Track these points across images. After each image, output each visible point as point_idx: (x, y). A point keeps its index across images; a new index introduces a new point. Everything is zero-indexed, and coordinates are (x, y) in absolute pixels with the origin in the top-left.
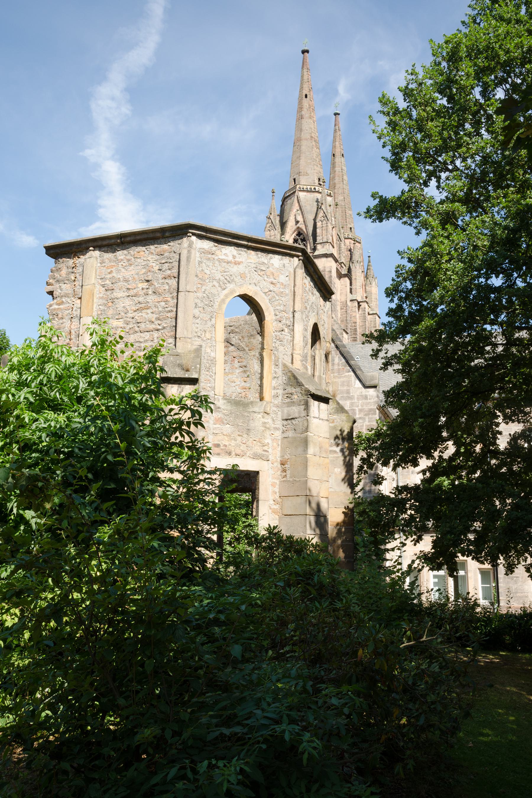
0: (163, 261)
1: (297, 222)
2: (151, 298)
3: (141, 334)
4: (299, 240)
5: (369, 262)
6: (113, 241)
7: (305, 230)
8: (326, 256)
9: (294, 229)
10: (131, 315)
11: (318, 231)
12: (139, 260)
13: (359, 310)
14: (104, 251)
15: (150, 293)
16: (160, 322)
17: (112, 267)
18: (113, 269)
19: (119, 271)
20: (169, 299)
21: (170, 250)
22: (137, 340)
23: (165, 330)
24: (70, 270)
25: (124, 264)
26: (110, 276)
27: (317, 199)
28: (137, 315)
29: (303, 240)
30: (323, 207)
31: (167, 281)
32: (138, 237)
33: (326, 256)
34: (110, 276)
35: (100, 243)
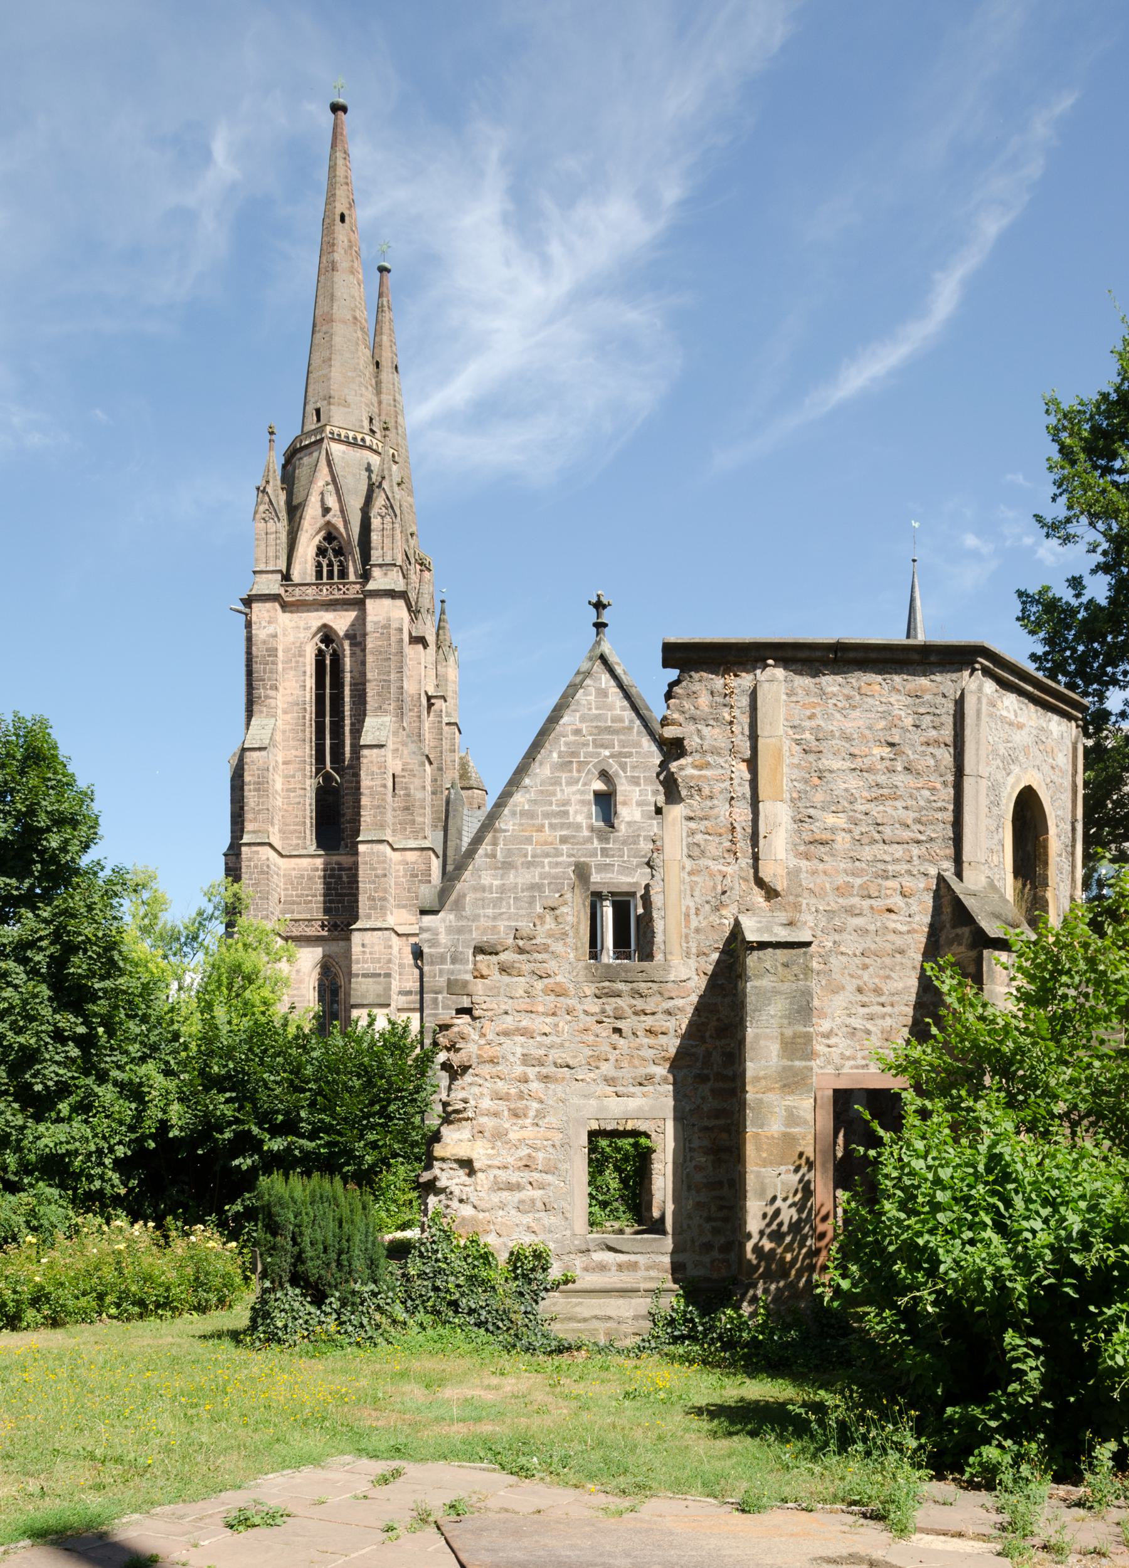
0: (922, 710)
1: (326, 510)
2: (901, 779)
3: (886, 847)
4: (330, 552)
5: (443, 612)
6: (818, 654)
7: (342, 530)
8: (391, 594)
9: (318, 525)
10: (863, 808)
11: (375, 537)
12: (869, 700)
13: (429, 713)
14: (796, 672)
15: (899, 769)
16: (922, 828)
17: (814, 705)
18: (817, 711)
19: (828, 717)
20: (938, 786)
21: (935, 690)
22: (879, 857)
23: (933, 844)
24: (719, 699)
25: (839, 704)
26: (813, 723)
27: (369, 464)
28: (875, 810)
29: (339, 552)
30: (385, 485)
31: (931, 749)
32: (873, 655)
33: (391, 594)
34: (813, 723)
35: (789, 654)
